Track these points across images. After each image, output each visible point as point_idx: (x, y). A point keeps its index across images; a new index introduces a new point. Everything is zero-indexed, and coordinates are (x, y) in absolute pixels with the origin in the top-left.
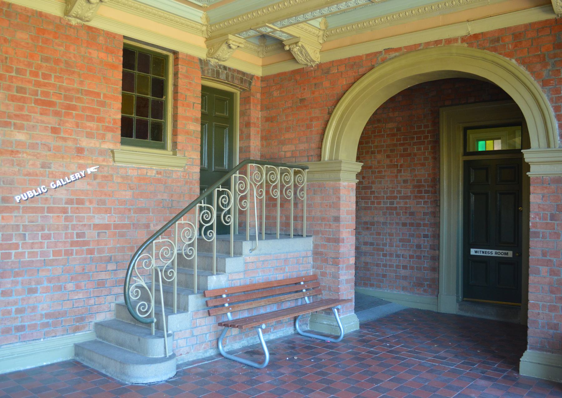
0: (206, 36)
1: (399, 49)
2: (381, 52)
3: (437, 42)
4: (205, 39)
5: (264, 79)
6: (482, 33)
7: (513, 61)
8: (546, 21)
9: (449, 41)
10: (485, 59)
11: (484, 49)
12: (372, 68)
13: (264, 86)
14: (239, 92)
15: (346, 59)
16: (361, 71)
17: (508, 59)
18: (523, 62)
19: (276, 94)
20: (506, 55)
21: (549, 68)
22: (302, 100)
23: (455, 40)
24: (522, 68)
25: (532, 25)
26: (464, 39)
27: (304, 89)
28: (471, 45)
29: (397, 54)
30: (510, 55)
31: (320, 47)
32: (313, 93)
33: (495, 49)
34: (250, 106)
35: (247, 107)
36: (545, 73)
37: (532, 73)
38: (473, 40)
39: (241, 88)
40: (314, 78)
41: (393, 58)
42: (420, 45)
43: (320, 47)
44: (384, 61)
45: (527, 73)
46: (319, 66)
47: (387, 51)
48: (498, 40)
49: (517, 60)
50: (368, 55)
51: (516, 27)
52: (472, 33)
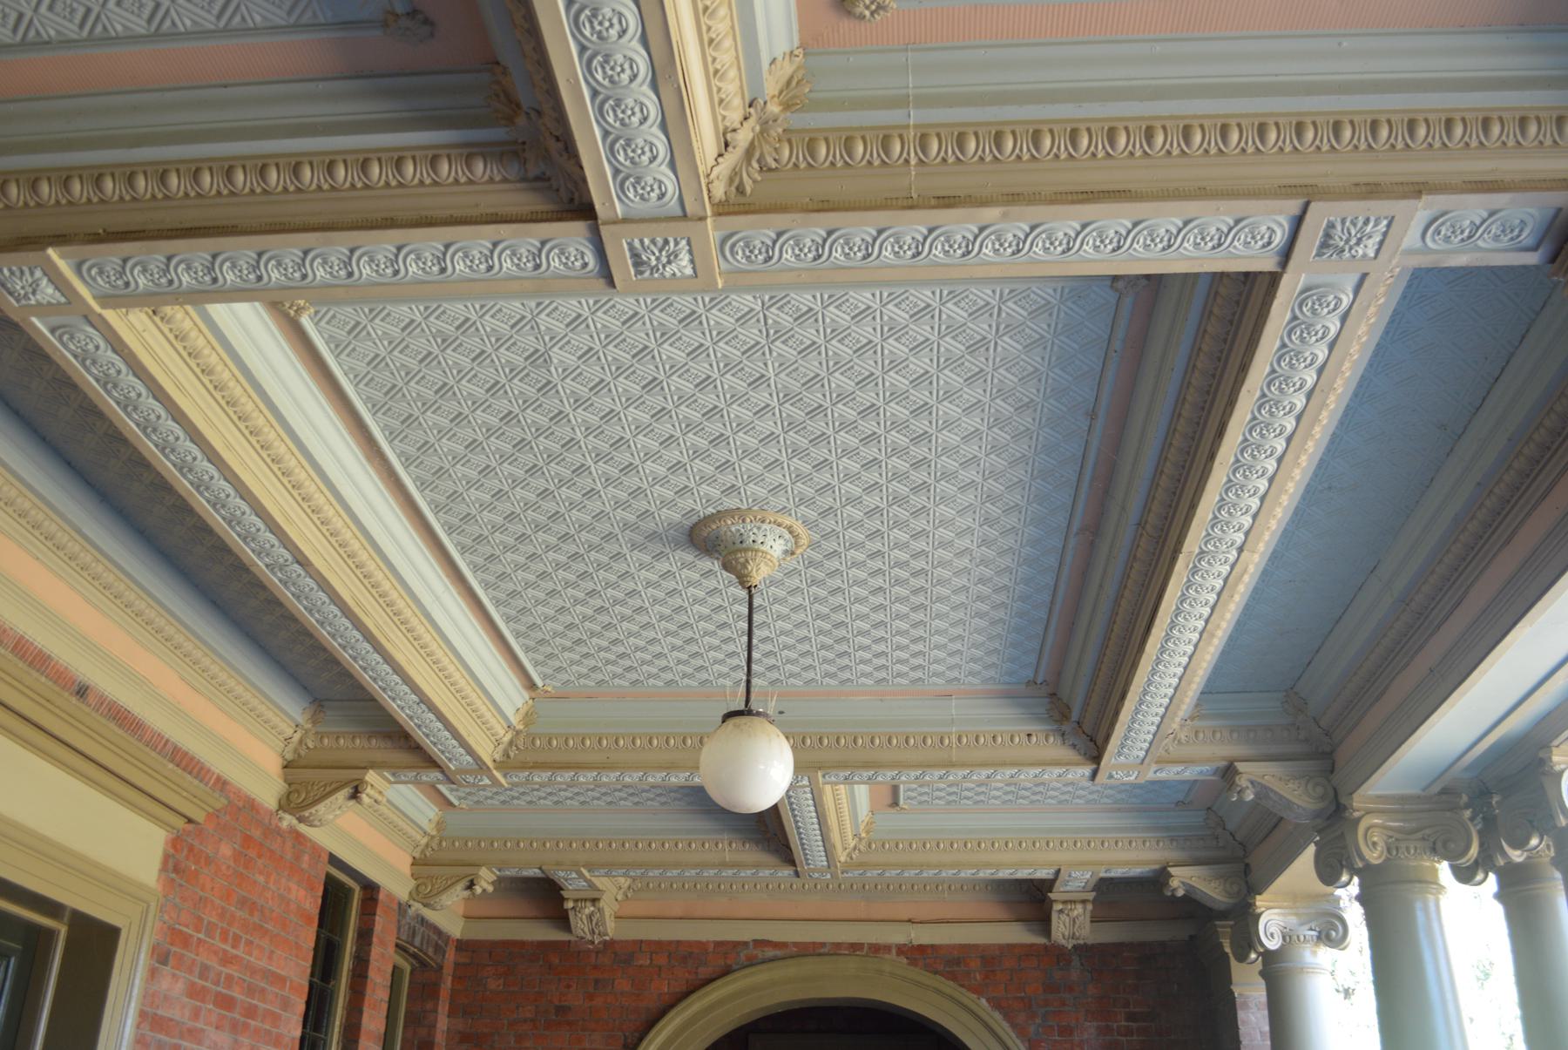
0: (417, 855)
1: (783, 945)
2: (745, 944)
3: (855, 947)
4: (410, 860)
5: (462, 945)
6: (933, 946)
7: (983, 1001)
8: (1032, 945)
9: (876, 949)
10: (938, 991)
11: (936, 973)
12: (726, 972)
13: (462, 960)
14: (408, 968)
15: (670, 943)
16: (704, 972)
17: (974, 996)
18: (997, 1004)
19: (494, 984)
20: (970, 989)
21: (1038, 1021)
22: (562, 1010)
23: (887, 948)
24: (997, 1015)
25: (1011, 947)
26: (902, 950)
27: (569, 986)
28: (913, 962)
29: (778, 953)
30: (977, 991)
31: (616, 907)
32: (591, 997)
33: (952, 977)
34: (437, 1004)
35: (429, 1006)
36: (1032, 1029)
37: (1013, 1026)
38: (917, 954)
39: (414, 956)
40: (595, 967)
41: (772, 960)
42: (823, 945)
43: (616, 907)
44: (752, 962)
45: (1005, 1025)
46: (609, 945)
47: (759, 943)
48: (958, 962)
49: (988, 1000)
50: (718, 944)
51: (989, 946)
52: (915, 943)
